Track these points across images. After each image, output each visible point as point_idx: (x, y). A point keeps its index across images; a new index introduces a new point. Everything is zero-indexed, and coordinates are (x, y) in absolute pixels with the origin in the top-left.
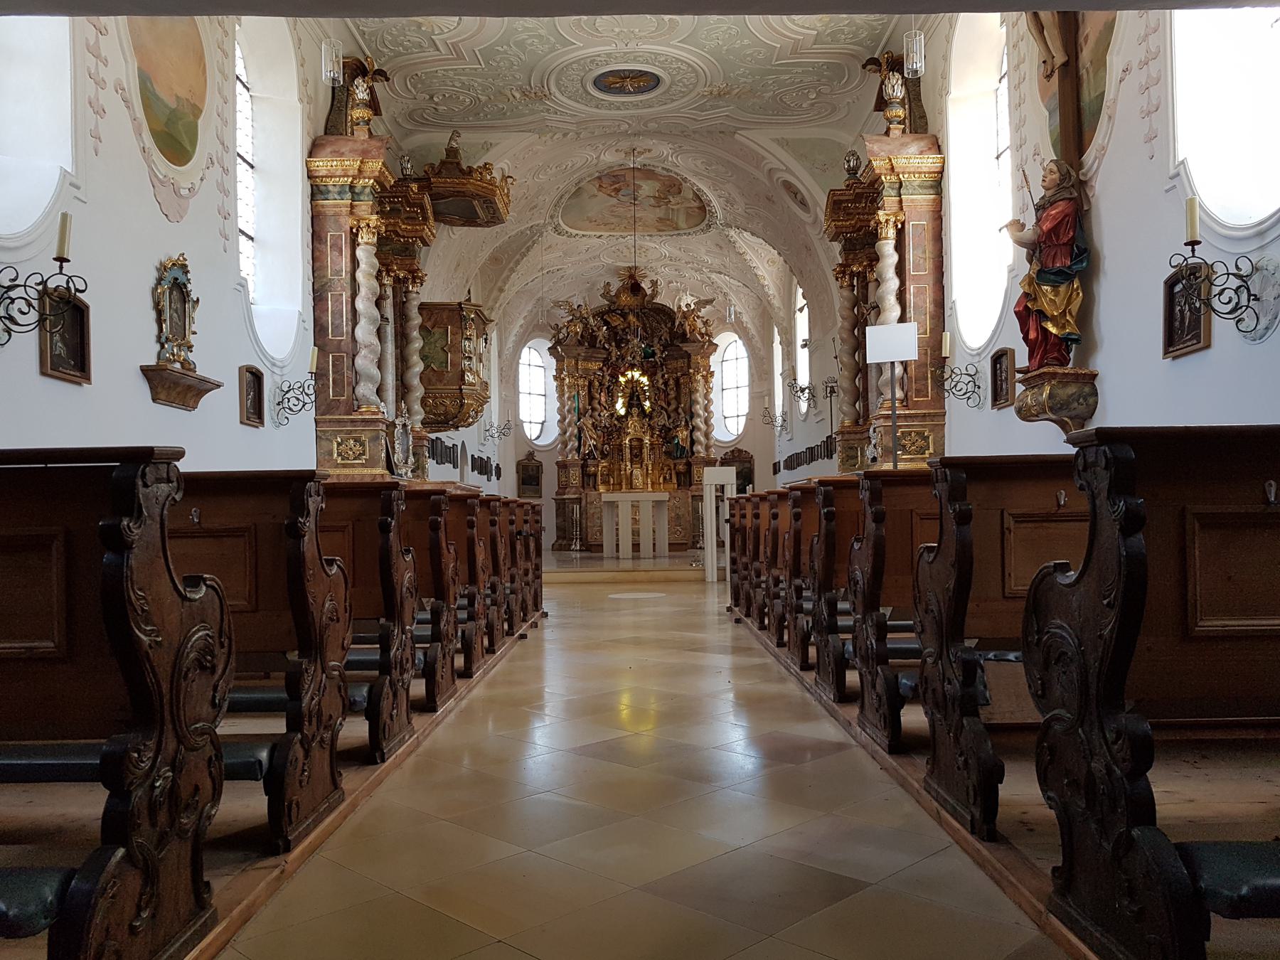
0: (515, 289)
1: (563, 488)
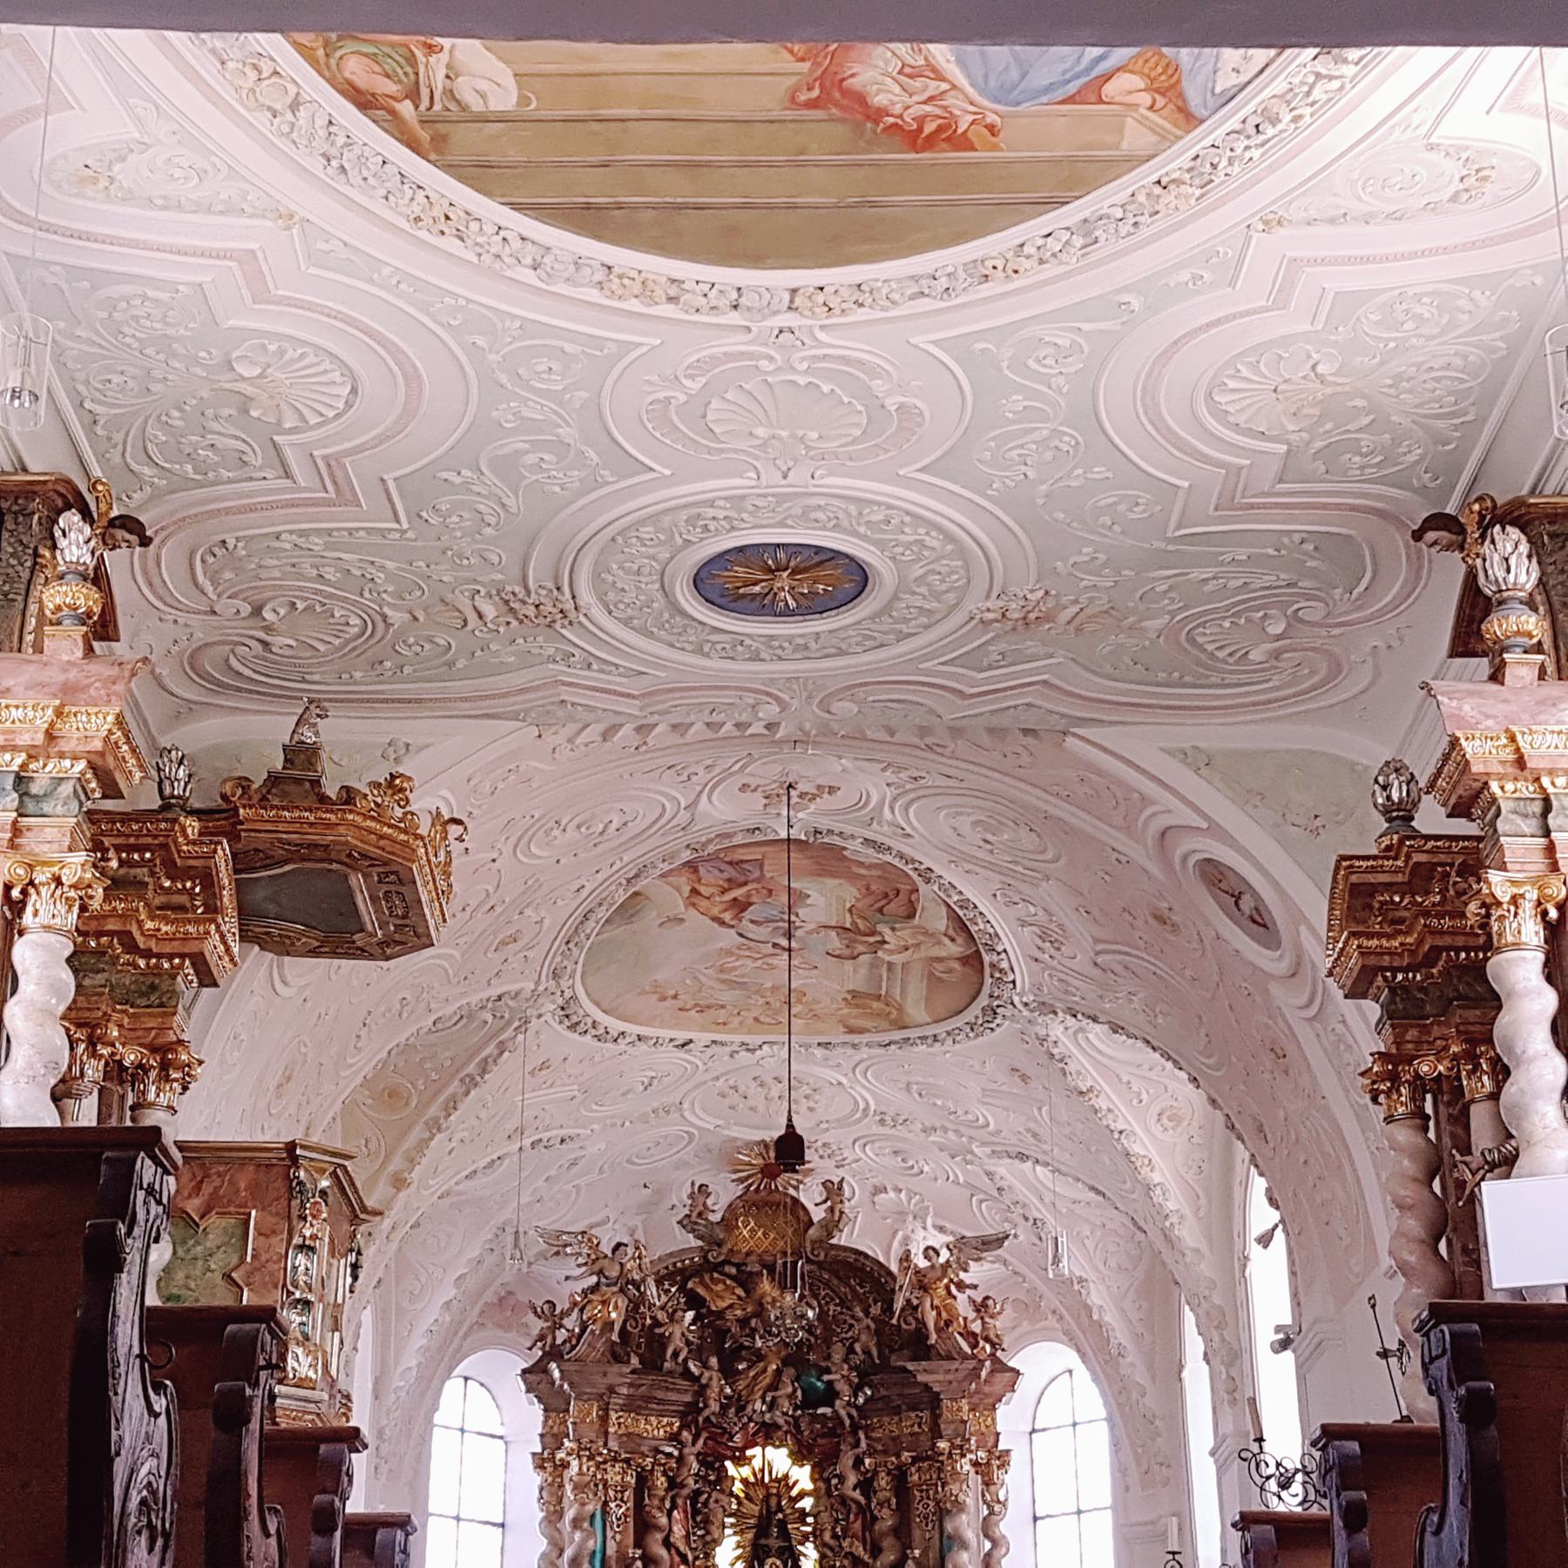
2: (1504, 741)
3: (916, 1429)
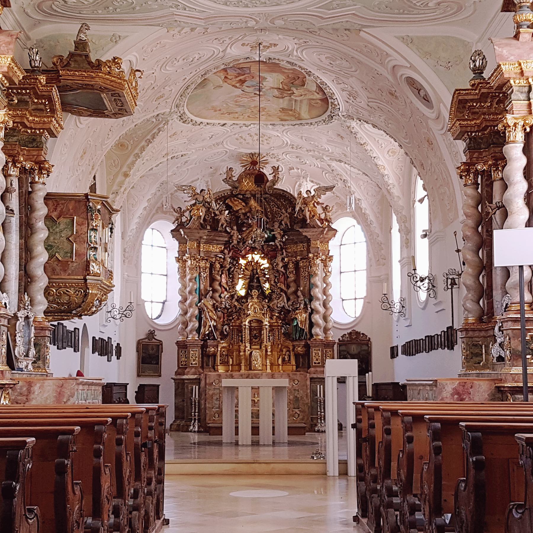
0: (139, 174)
1: (182, 368)
2: (517, 65)
3: (302, 249)
